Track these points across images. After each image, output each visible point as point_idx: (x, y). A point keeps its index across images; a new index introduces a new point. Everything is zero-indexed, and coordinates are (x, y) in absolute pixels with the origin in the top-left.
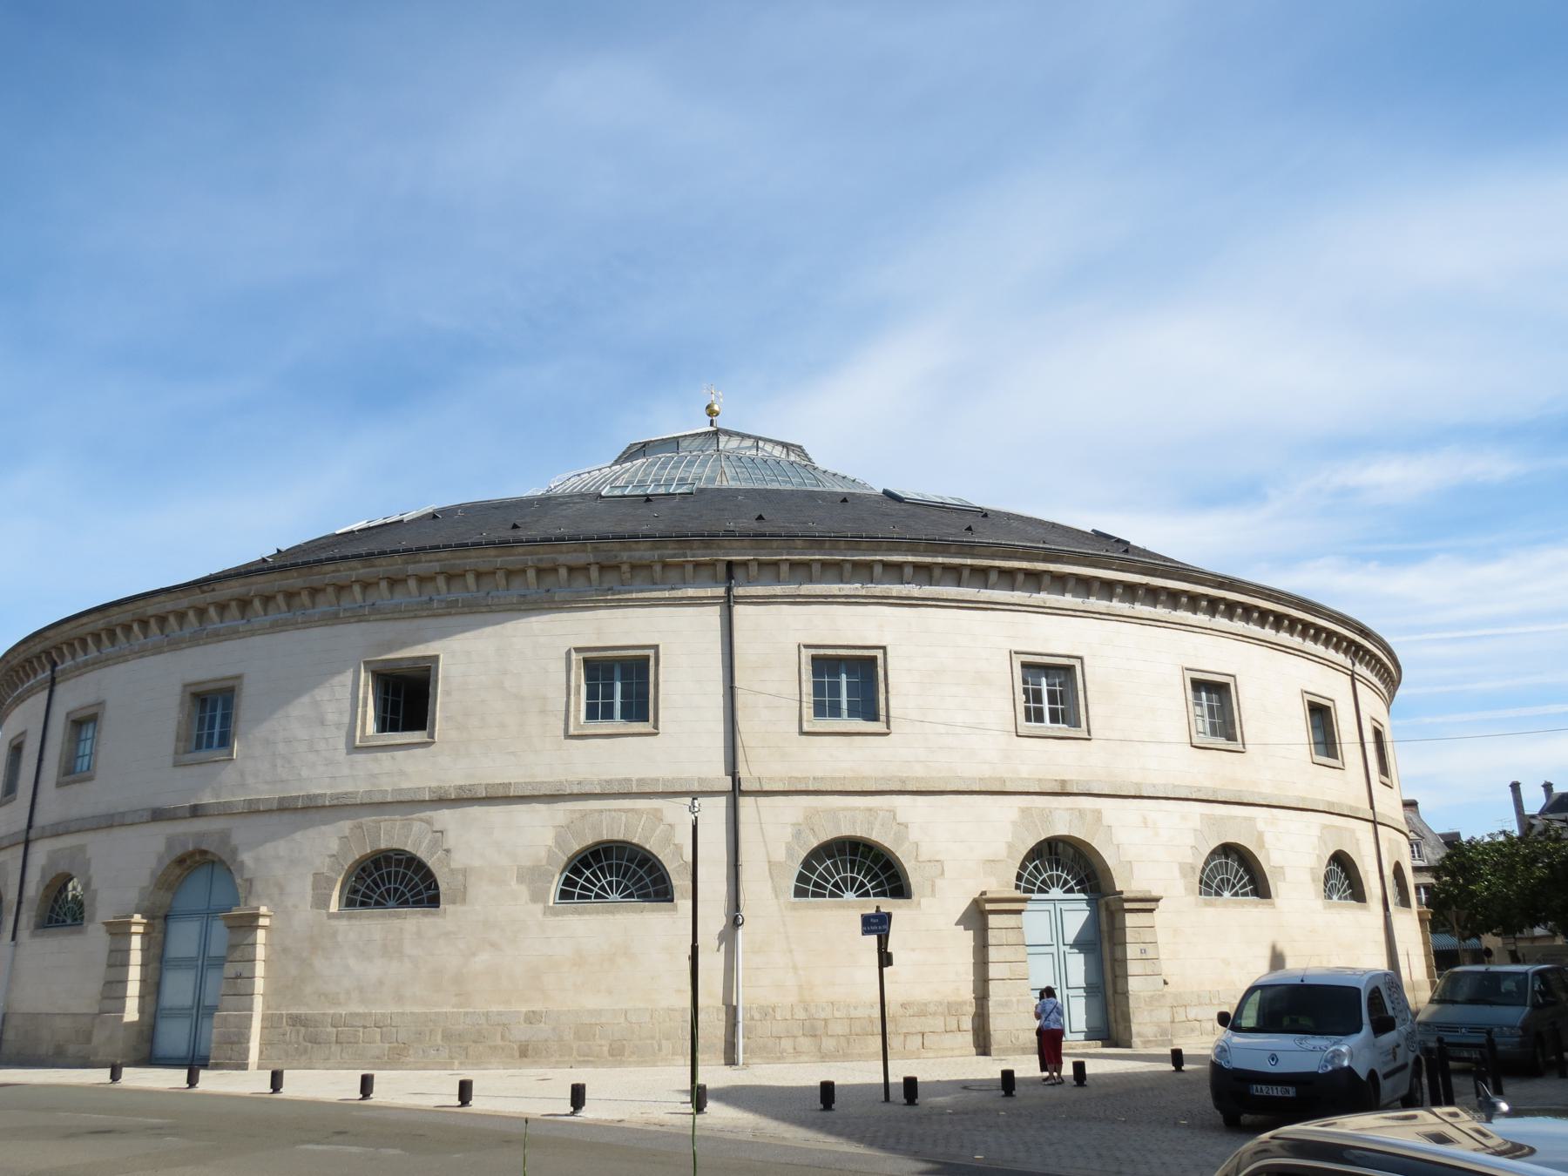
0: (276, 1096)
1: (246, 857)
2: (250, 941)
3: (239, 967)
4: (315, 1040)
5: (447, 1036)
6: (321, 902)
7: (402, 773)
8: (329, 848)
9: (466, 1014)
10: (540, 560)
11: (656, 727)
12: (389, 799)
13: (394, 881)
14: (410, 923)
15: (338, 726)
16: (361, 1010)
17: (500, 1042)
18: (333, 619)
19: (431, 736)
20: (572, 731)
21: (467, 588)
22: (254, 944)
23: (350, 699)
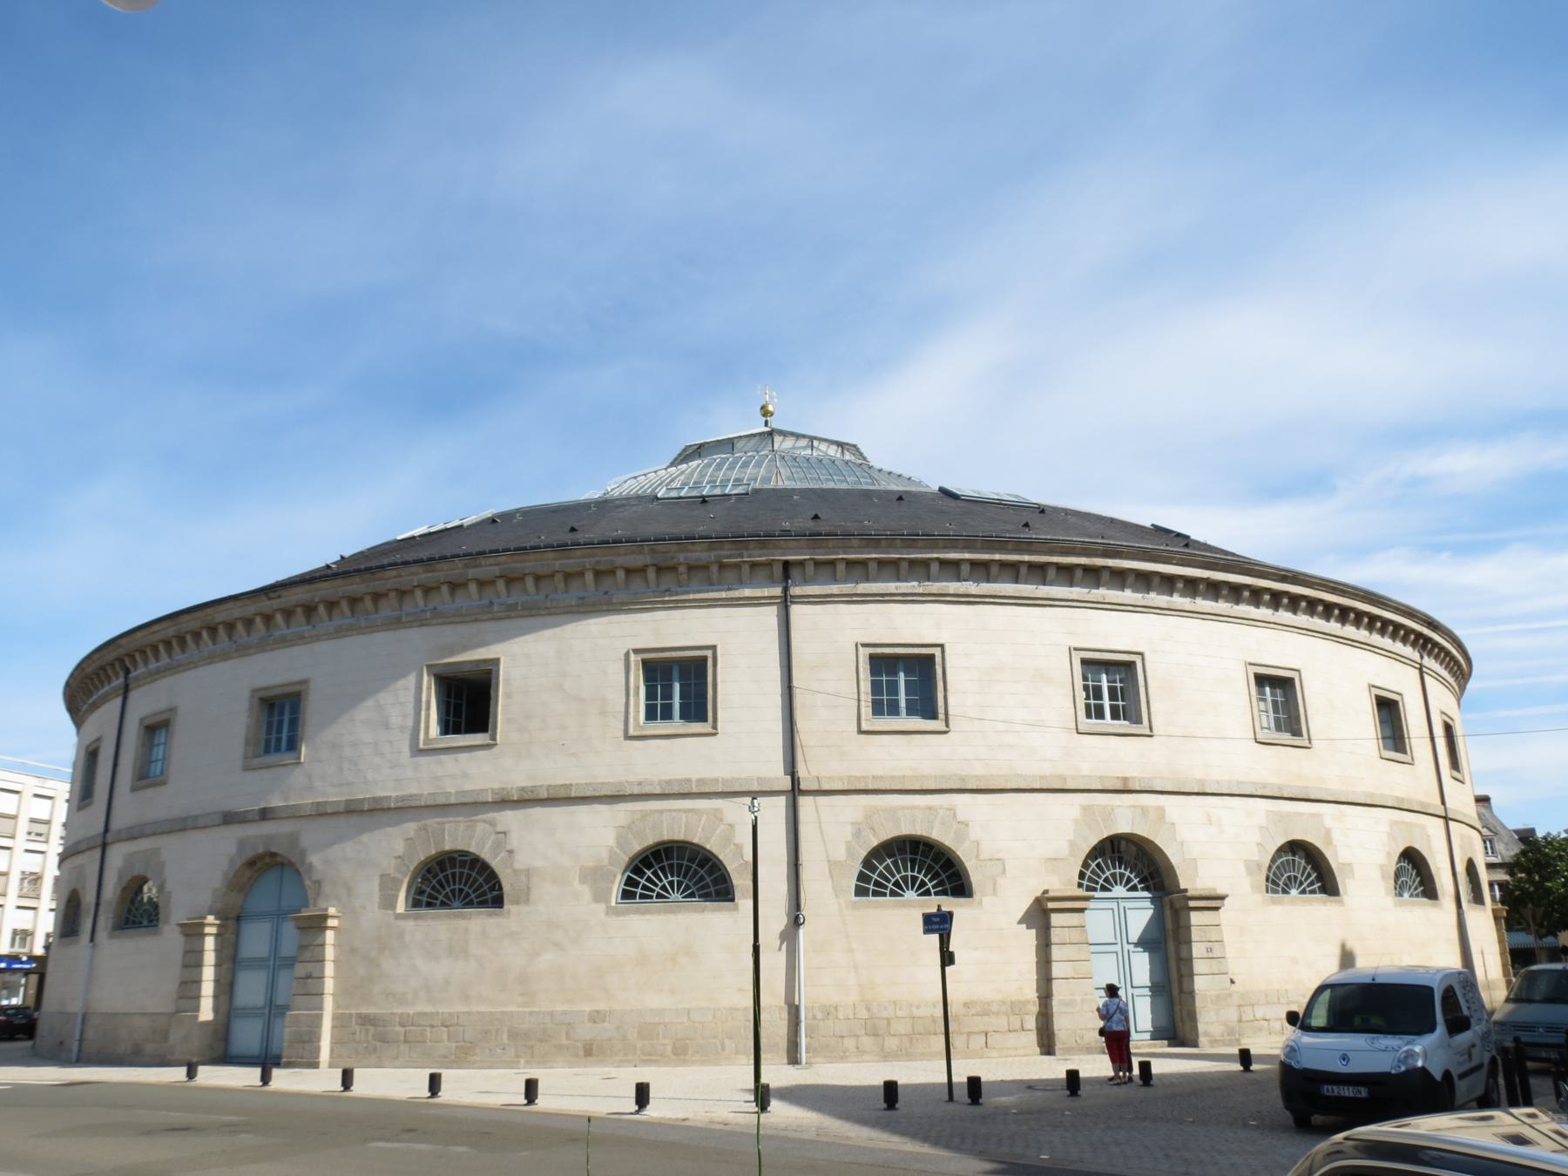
0: (347, 1094)
1: (315, 859)
2: (318, 941)
3: (310, 967)
4: (383, 1039)
5: (513, 1035)
6: (388, 902)
7: (465, 775)
8: (395, 850)
9: (531, 1013)
10: (598, 562)
11: (715, 727)
12: (453, 801)
13: (459, 883)
14: (475, 923)
15: (402, 729)
16: (428, 1009)
17: (564, 1041)
18: (396, 623)
19: (493, 738)
20: (632, 732)
21: (525, 592)
22: (323, 945)
23: (414, 702)
